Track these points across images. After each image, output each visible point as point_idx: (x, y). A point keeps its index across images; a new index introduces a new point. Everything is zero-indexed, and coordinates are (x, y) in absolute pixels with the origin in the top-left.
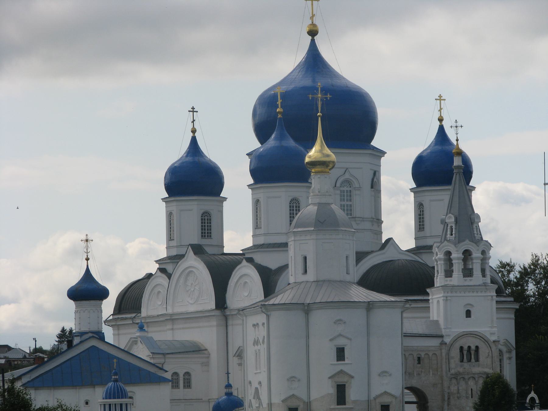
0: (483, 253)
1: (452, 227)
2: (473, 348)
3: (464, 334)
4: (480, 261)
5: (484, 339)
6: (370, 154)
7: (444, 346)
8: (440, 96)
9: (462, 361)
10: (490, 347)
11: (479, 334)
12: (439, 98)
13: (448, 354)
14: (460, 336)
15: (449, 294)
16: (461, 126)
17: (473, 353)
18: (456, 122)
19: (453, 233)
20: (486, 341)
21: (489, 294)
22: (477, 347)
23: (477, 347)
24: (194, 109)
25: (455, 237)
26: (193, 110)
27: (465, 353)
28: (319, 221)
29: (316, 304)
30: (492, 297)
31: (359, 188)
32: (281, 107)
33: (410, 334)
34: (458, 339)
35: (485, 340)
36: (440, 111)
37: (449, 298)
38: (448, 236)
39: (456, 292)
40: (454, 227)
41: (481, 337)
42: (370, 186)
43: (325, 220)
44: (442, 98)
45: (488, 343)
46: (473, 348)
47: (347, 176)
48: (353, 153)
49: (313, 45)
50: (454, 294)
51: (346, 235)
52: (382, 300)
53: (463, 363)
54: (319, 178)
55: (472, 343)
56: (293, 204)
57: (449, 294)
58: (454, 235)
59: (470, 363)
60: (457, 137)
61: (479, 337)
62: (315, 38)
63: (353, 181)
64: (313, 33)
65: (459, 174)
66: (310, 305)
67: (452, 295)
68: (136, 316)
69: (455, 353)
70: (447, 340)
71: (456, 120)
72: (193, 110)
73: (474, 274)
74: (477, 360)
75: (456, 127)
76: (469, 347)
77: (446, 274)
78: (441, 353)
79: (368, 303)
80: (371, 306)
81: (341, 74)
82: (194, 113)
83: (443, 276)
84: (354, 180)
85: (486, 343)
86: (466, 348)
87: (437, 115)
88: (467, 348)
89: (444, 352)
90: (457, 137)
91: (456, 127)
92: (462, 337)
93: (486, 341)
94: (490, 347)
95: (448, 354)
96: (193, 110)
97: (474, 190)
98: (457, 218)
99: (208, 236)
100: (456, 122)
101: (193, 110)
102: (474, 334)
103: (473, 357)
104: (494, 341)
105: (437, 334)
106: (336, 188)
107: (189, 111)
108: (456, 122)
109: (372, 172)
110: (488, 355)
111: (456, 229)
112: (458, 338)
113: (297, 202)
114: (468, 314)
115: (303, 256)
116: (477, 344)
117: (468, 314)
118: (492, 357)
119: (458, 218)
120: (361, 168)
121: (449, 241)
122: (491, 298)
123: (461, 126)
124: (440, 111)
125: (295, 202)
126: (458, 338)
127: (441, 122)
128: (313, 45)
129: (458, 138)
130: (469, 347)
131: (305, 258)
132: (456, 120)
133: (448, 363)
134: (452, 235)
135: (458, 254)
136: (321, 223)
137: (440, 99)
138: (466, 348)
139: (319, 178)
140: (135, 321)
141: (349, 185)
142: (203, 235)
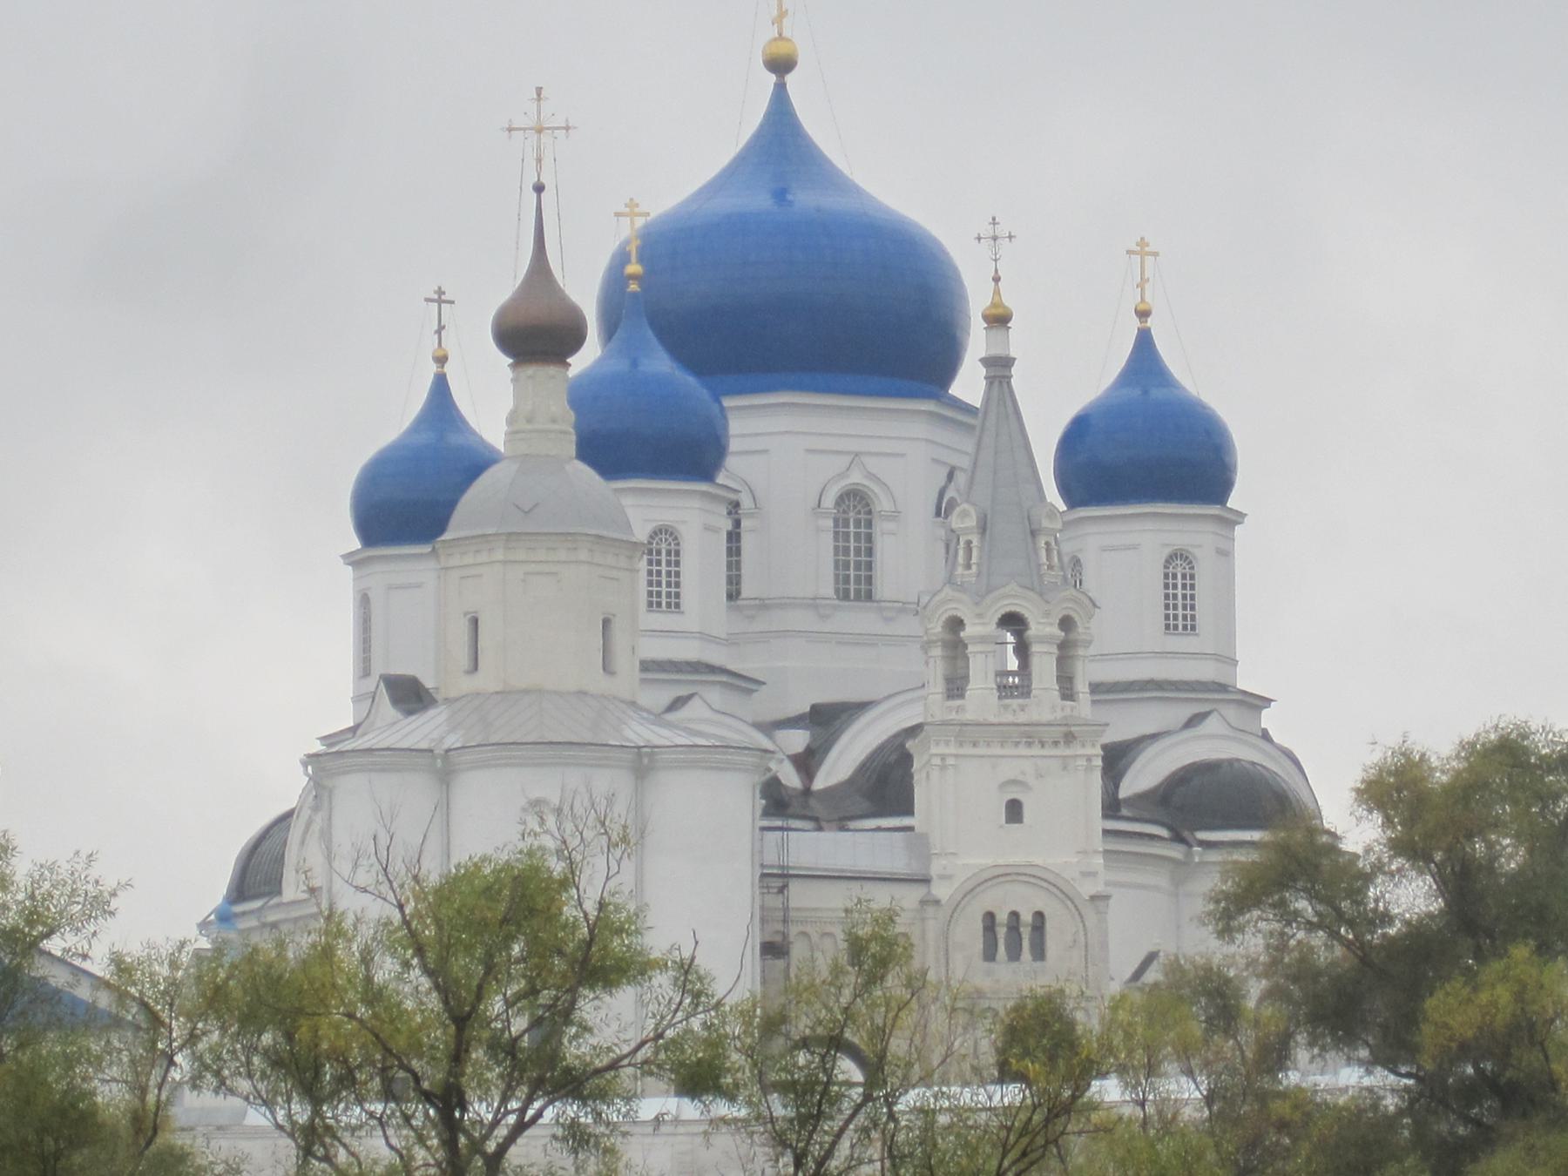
0: (1066, 623)
1: (969, 543)
2: (1027, 917)
3: (996, 874)
4: (1054, 650)
5: (1061, 891)
6: (931, 414)
7: (930, 910)
8: (1142, 243)
9: (990, 954)
10: (1082, 917)
11: (1051, 878)
12: (436, 297)
13: (946, 935)
14: (986, 881)
15: (952, 750)
16: (1010, 237)
17: (1026, 933)
18: (994, 222)
19: (974, 560)
20: (1066, 896)
21: (1081, 751)
22: (1039, 916)
23: (1039, 916)
24: (444, 293)
25: (979, 575)
26: (440, 298)
27: (1002, 932)
28: (517, 506)
29: (467, 750)
30: (1089, 759)
31: (895, 516)
32: (641, 260)
33: (809, 869)
34: (978, 889)
35: (1063, 893)
36: (1141, 285)
37: (950, 761)
38: (960, 570)
39: (975, 745)
40: (975, 543)
41: (1050, 883)
42: (932, 509)
43: (536, 505)
44: (636, 210)
45: (1073, 903)
46: (1027, 917)
47: (856, 478)
48: (865, 408)
49: (780, 96)
50: (968, 750)
51: (617, 555)
52: (679, 743)
53: (992, 965)
54: (530, 377)
55: (1026, 902)
56: (657, 544)
57: (952, 750)
58: (974, 568)
59: (1015, 965)
60: (996, 271)
61: (1045, 885)
62: (790, 79)
63: (873, 491)
64: (781, 65)
65: (1000, 382)
66: (452, 753)
67: (962, 751)
68: (266, 903)
69: (969, 933)
70: (941, 891)
71: (994, 219)
72: (440, 297)
73: (1033, 687)
74: (1039, 953)
75: (995, 238)
76: (1015, 915)
77: (948, 690)
78: (924, 932)
79: (636, 750)
80: (646, 761)
81: (850, 177)
82: (443, 305)
83: (940, 696)
84: (876, 489)
85: (1069, 903)
86: (1002, 917)
87: (1131, 301)
88: (1006, 917)
89: (933, 928)
90: (996, 271)
91: (995, 238)
92: (990, 883)
93: (1067, 896)
94: (1082, 917)
95: (946, 935)
96: (440, 297)
97: (1240, 523)
98: (986, 516)
99: (669, 605)
100: (994, 222)
101: (440, 298)
102: (1030, 875)
103: (1026, 944)
104: (1093, 898)
105: (895, 871)
106: (820, 510)
107: (428, 300)
108: (994, 224)
109: (944, 472)
110: (1075, 941)
111: (981, 549)
112: (979, 885)
113: (670, 539)
114: (1014, 811)
115: (469, 616)
116: (1039, 907)
117: (1014, 811)
118: (1086, 946)
119: (989, 517)
120: (903, 455)
121: (962, 588)
122: (1085, 763)
123: (1010, 237)
124: (1141, 285)
125: (666, 540)
126: (979, 885)
127: (1143, 319)
128: (780, 96)
129: (1000, 273)
130: (1015, 915)
131: (475, 622)
132: (994, 219)
133: (943, 961)
134: (968, 566)
135: (983, 624)
136: (523, 511)
137: (1142, 250)
138: (1002, 917)
139: (530, 377)
140: (265, 917)
141: (863, 507)
142: (670, 572)
